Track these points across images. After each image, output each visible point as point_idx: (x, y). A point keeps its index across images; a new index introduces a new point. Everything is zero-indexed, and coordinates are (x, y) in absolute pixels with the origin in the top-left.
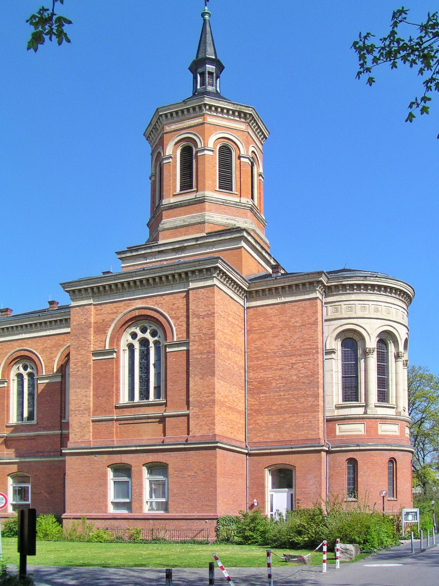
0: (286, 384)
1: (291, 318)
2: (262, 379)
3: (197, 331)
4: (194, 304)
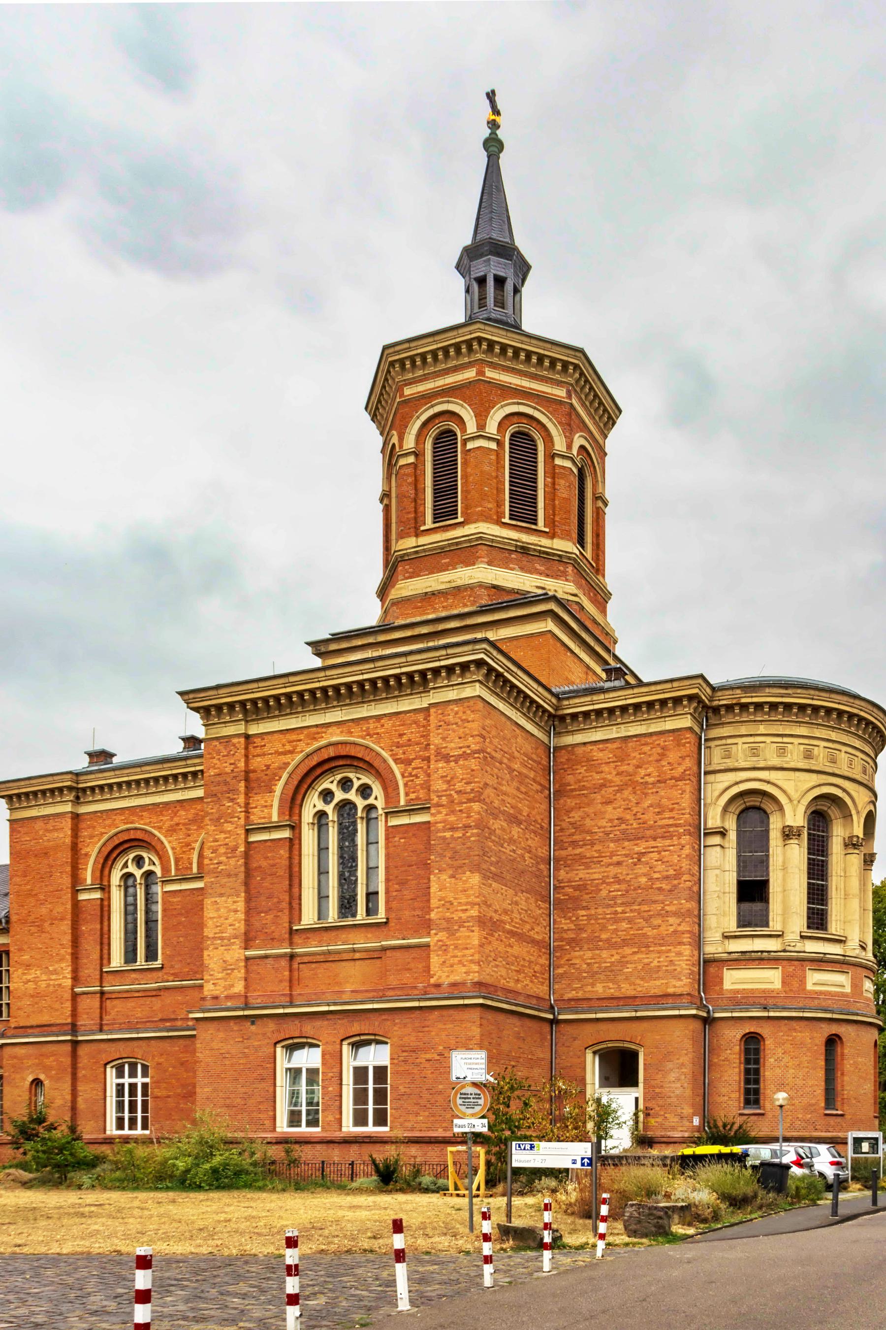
0: (627, 891)
1: (638, 767)
2: (581, 883)
3: (445, 787)
4: (438, 734)
